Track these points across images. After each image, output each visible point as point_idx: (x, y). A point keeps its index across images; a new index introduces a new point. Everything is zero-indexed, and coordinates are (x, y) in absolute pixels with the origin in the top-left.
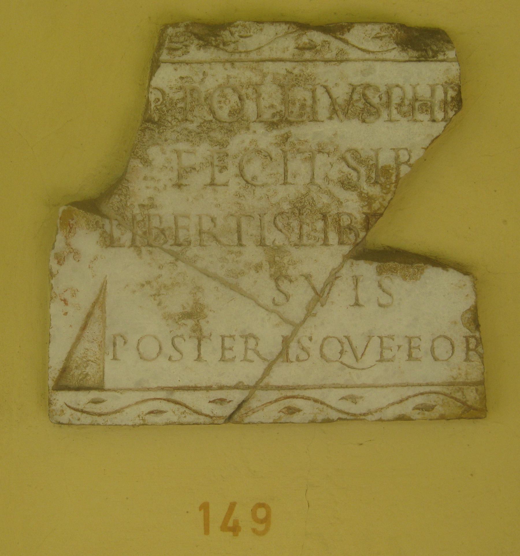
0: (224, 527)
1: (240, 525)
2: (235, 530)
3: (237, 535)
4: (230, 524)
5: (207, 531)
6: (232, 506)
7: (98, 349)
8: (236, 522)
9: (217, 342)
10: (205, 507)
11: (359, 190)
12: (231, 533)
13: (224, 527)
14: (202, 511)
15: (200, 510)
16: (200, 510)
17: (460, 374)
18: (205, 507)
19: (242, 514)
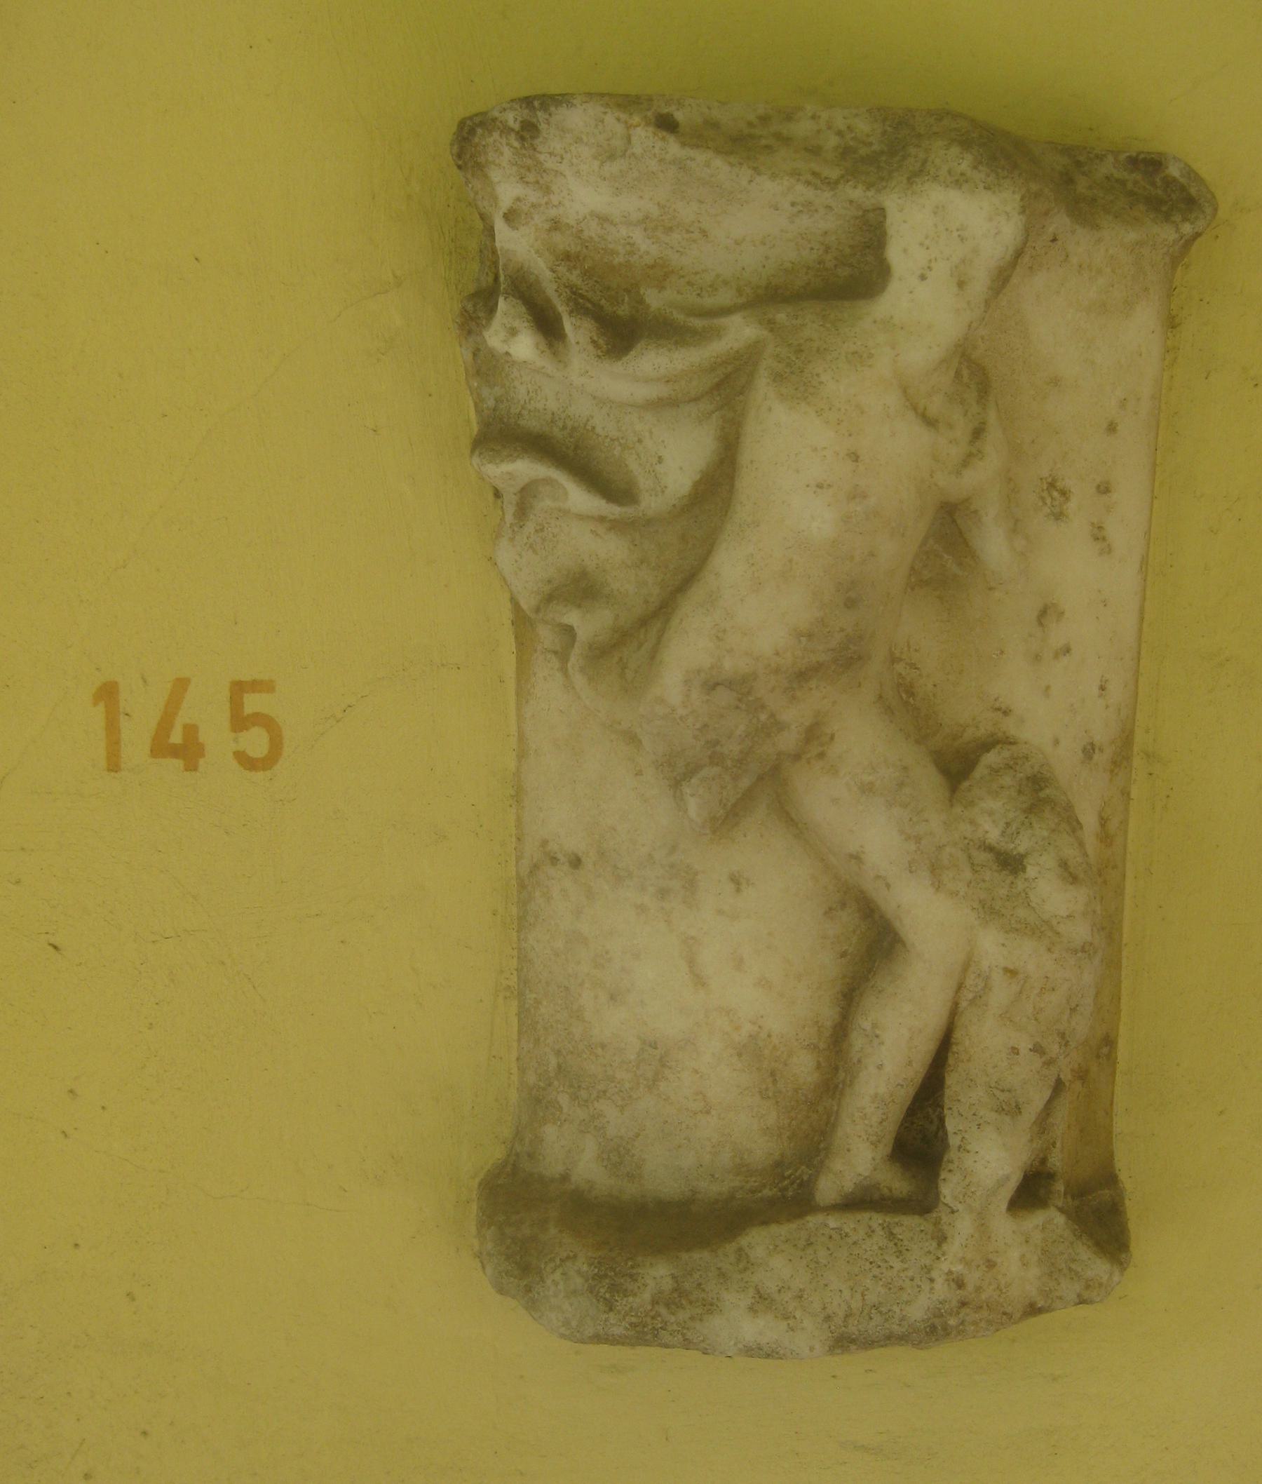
0: (161, 748)
1: (201, 740)
2: (189, 752)
3: (195, 769)
4: (176, 738)
5: (114, 765)
6: (181, 685)
7: (1036, 1258)
8: (191, 731)
9: (689, 648)
10: (108, 694)
11: (729, 763)
12: (178, 763)
13: (161, 748)
14: (101, 708)
15: (95, 704)
16: (95, 704)
17: (901, 211)
18: (108, 694)
19: (207, 713)
